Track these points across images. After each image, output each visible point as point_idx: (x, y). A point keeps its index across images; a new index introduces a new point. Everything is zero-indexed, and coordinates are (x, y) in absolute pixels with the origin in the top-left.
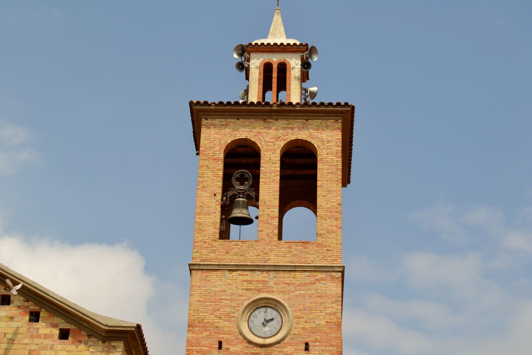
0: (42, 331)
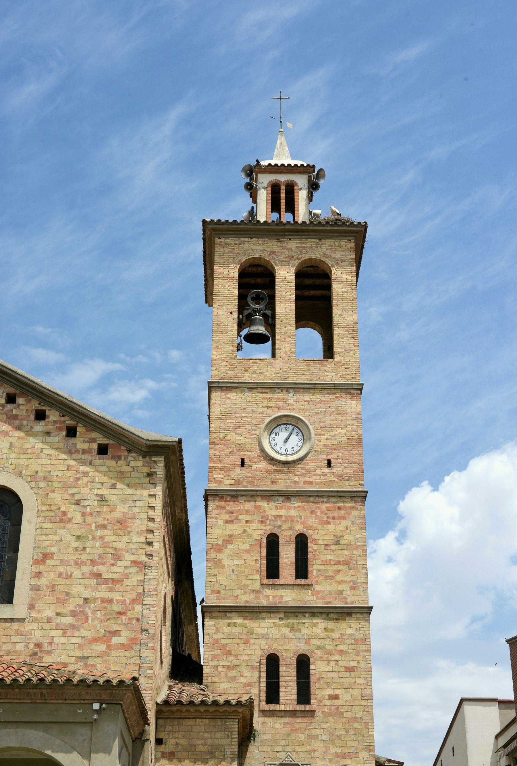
0: (81, 446)
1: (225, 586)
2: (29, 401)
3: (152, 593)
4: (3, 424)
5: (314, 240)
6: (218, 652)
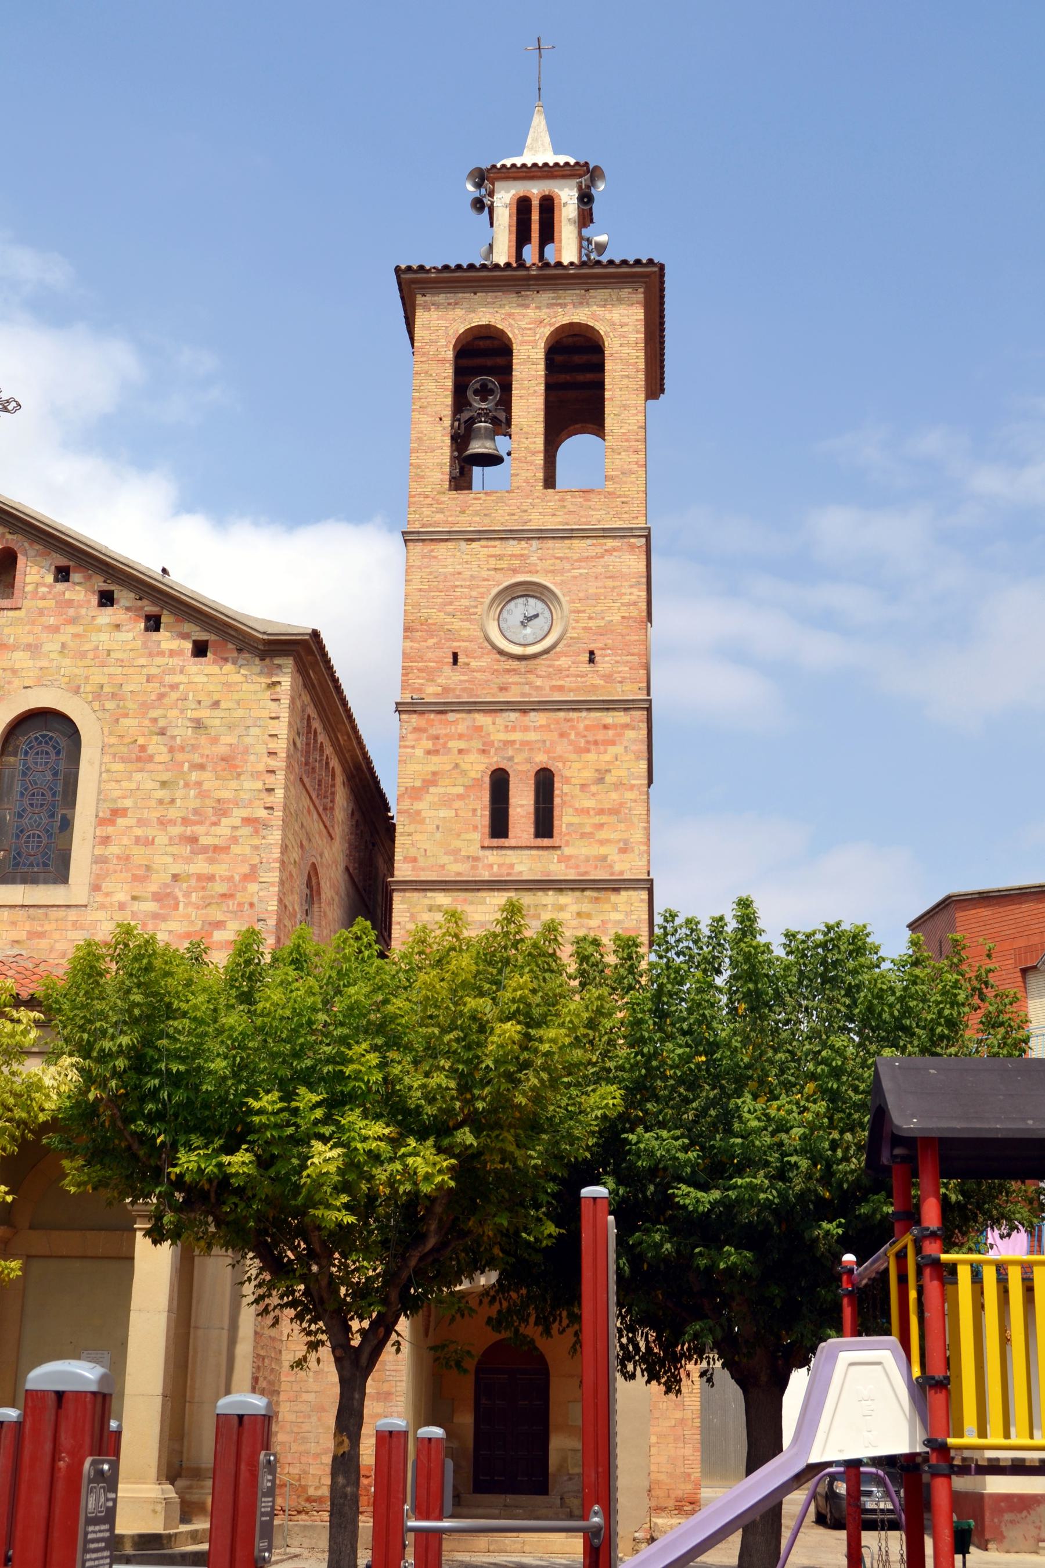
1: (426, 850)
5: (578, 292)
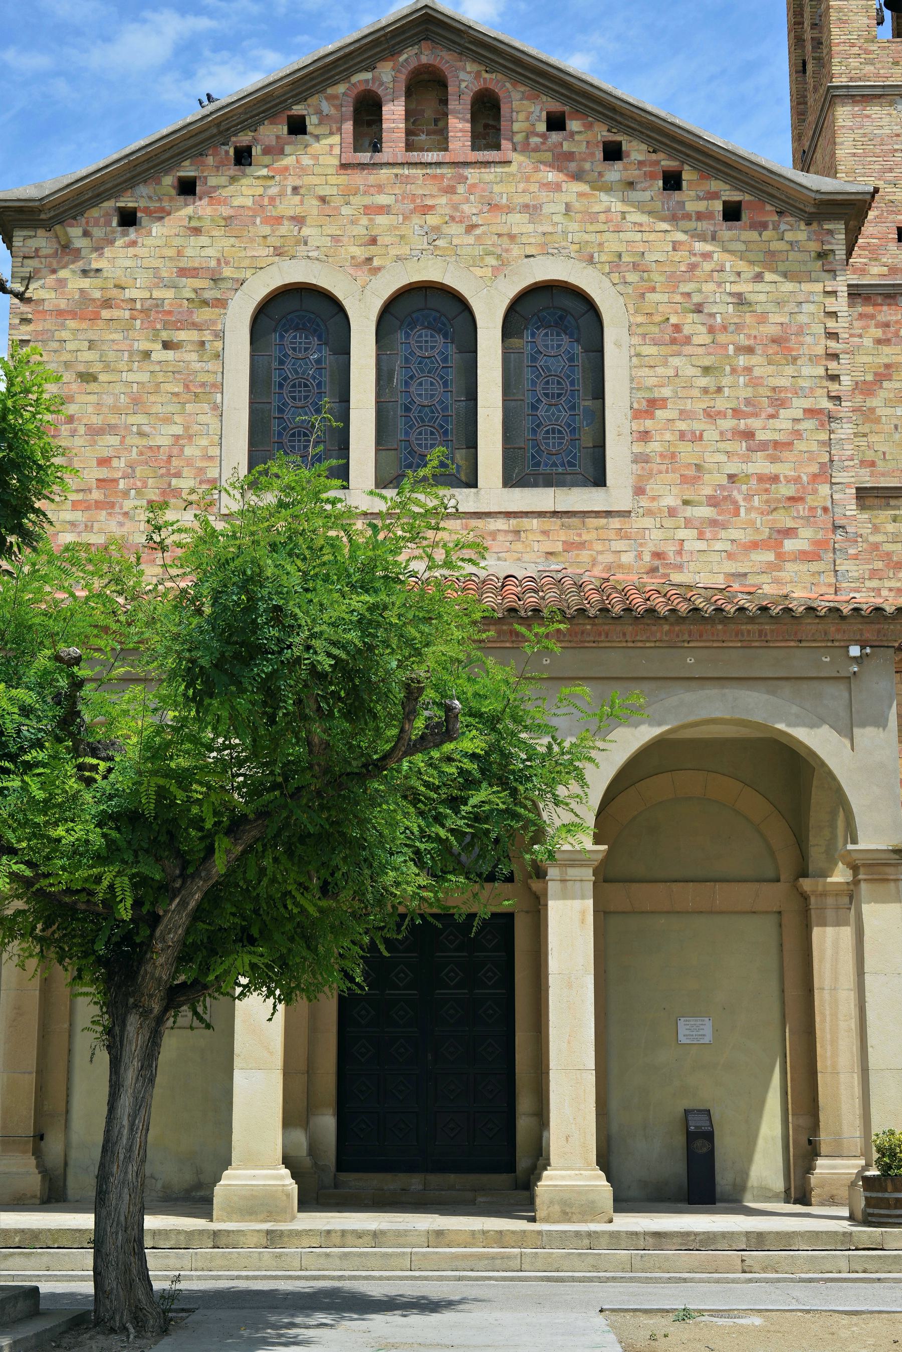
0: (692, 207)
1: (884, 453)
2: (589, 126)
3: (846, 463)
4: (548, 169)
6: (879, 565)
